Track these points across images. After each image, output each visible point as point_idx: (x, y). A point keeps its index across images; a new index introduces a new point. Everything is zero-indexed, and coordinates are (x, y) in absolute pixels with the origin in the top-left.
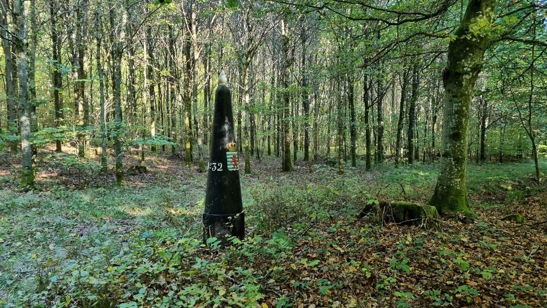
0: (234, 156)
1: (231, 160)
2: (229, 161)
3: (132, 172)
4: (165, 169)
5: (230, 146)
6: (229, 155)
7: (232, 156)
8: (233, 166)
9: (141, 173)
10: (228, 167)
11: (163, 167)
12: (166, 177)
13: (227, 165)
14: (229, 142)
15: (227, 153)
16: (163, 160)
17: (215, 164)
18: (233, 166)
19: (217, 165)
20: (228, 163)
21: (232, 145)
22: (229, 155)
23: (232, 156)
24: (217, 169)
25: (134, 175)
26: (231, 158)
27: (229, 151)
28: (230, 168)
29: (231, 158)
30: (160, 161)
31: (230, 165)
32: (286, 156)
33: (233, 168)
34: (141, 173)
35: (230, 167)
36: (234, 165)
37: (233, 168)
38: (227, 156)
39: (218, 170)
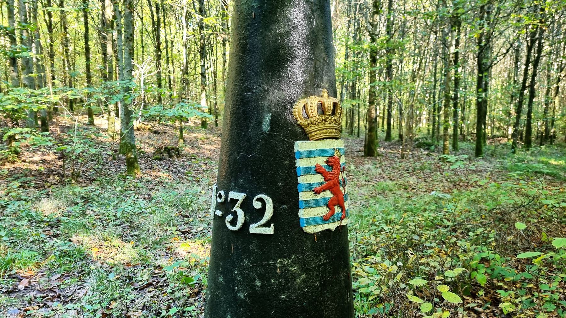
0: (332, 163)
1: (319, 178)
2: (307, 188)
3: (160, 156)
4: (210, 150)
5: (314, 112)
6: (307, 155)
7: (321, 161)
8: (323, 211)
9: (171, 157)
10: (303, 214)
11: (208, 147)
12: (206, 164)
13: (295, 205)
14: (307, 94)
15: (300, 146)
16: (211, 136)
17: (240, 196)
18: (323, 211)
19: (246, 205)
20: (304, 196)
21: (321, 108)
22: (307, 155)
23: (321, 161)
24: (246, 225)
25: (160, 160)
26: (318, 170)
27: (306, 137)
28: (313, 221)
29: (318, 170)
30: (208, 139)
31: (311, 204)
32: (370, 136)
33: (325, 219)
34: (171, 157)
35: (313, 217)
36: (330, 205)
37: (325, 219)
38: (300, 163)
39: (254, 229)
